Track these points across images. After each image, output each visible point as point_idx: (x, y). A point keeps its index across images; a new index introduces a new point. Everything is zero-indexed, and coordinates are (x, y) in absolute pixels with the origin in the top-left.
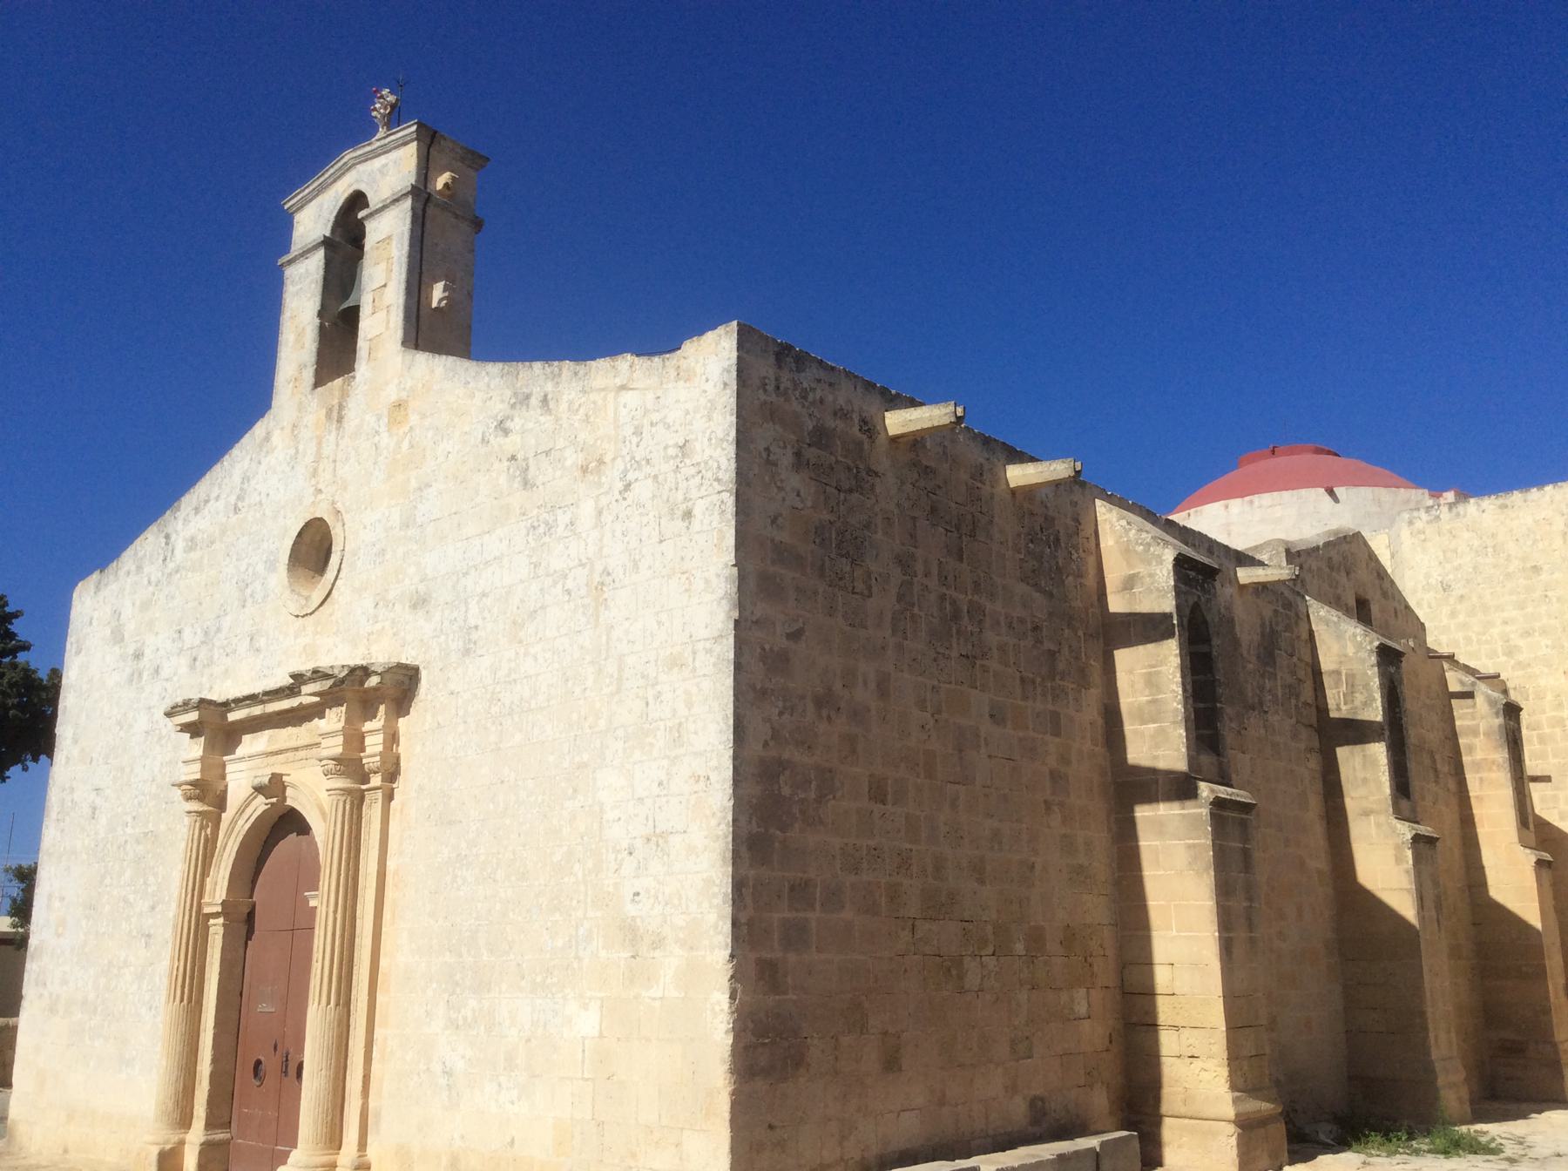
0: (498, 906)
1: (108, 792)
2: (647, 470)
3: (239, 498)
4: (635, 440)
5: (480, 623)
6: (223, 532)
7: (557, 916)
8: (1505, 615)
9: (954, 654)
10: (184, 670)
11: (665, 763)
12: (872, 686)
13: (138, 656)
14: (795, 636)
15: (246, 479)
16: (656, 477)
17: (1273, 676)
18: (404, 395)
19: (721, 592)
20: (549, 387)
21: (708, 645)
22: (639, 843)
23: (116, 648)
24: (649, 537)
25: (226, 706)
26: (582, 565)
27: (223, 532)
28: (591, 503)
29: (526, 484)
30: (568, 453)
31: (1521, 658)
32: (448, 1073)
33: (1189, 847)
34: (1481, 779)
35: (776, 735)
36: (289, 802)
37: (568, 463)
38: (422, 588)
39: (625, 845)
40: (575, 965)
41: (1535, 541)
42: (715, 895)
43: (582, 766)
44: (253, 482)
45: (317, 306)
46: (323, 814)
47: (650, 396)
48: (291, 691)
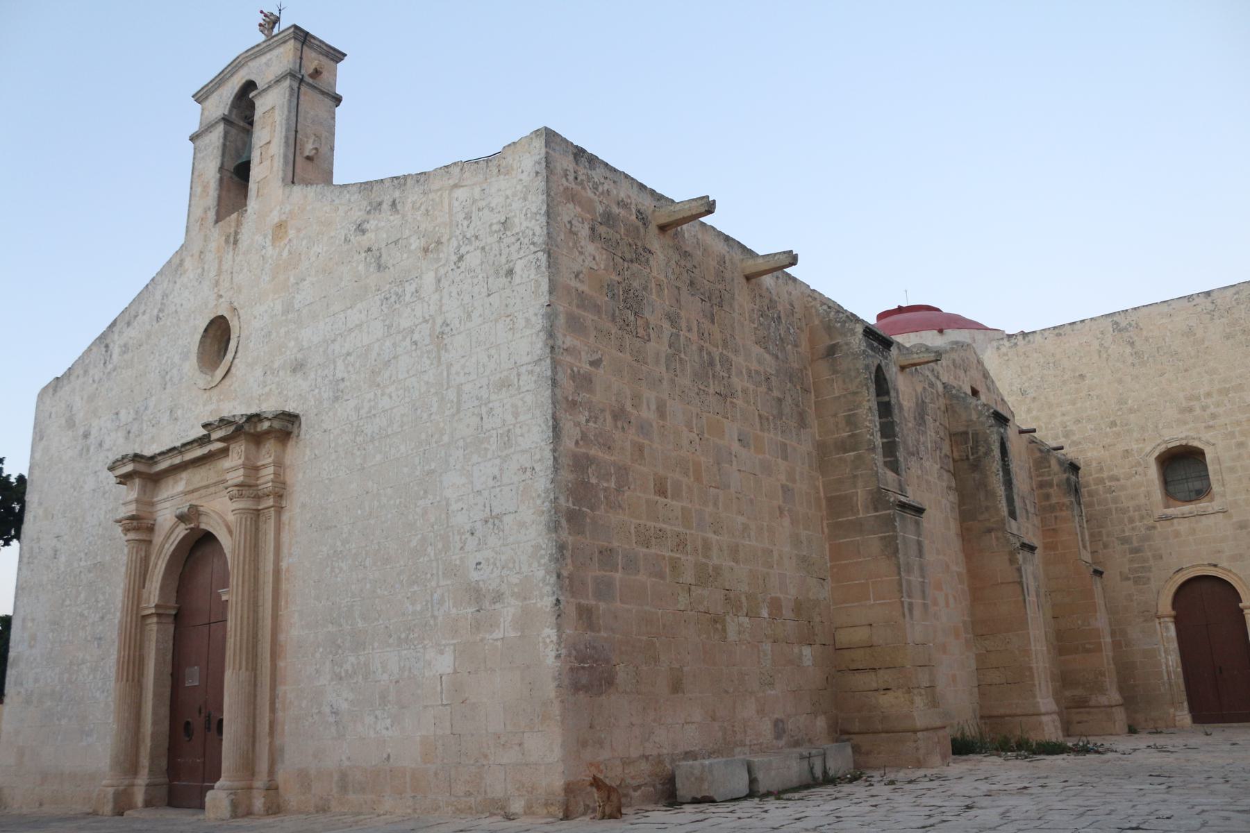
0: (368, 586)
1: (65, 538)
2: (477, 243)
3: (161, 310)
4: (466, 223)
5: (346, 375)
6: (149, 337)
7: (415, 588)
8: (1063, 409)
9: (711, 391)
10: (121, 441)
11: (498, 461)
12: (653, 407)
13: (86, 436)
14: (595, 364)
15: (165, 296)
16: (483, 248)
17: (925, 433)
18: (284, 217)
19: (539, 327)
20: (397, 194)
21: (530, 368)
22: (478, 525)
23: (70, 433)
24: (480, 293)
25: (152, 459)
26: (427, 321)
27: (149, 337)
28: (431, 274)
29: (380, 267)
30: (412, 240)
31: (1075, 438)
32: (335, 713)
33: (882, 538)
34: (1056, 517)
35: (584, 436)
36: (203, 526)
37: (413, 247)
38: (299, 356)
39: (467, 527)
40: (432, 622)
41: (1081, 358)
42: (542, 557)
43: (432, 472)
44: (171, 297)
45: (218, 165)
46: (230, 532)
47: (477, 190)
48: (203, 441)
